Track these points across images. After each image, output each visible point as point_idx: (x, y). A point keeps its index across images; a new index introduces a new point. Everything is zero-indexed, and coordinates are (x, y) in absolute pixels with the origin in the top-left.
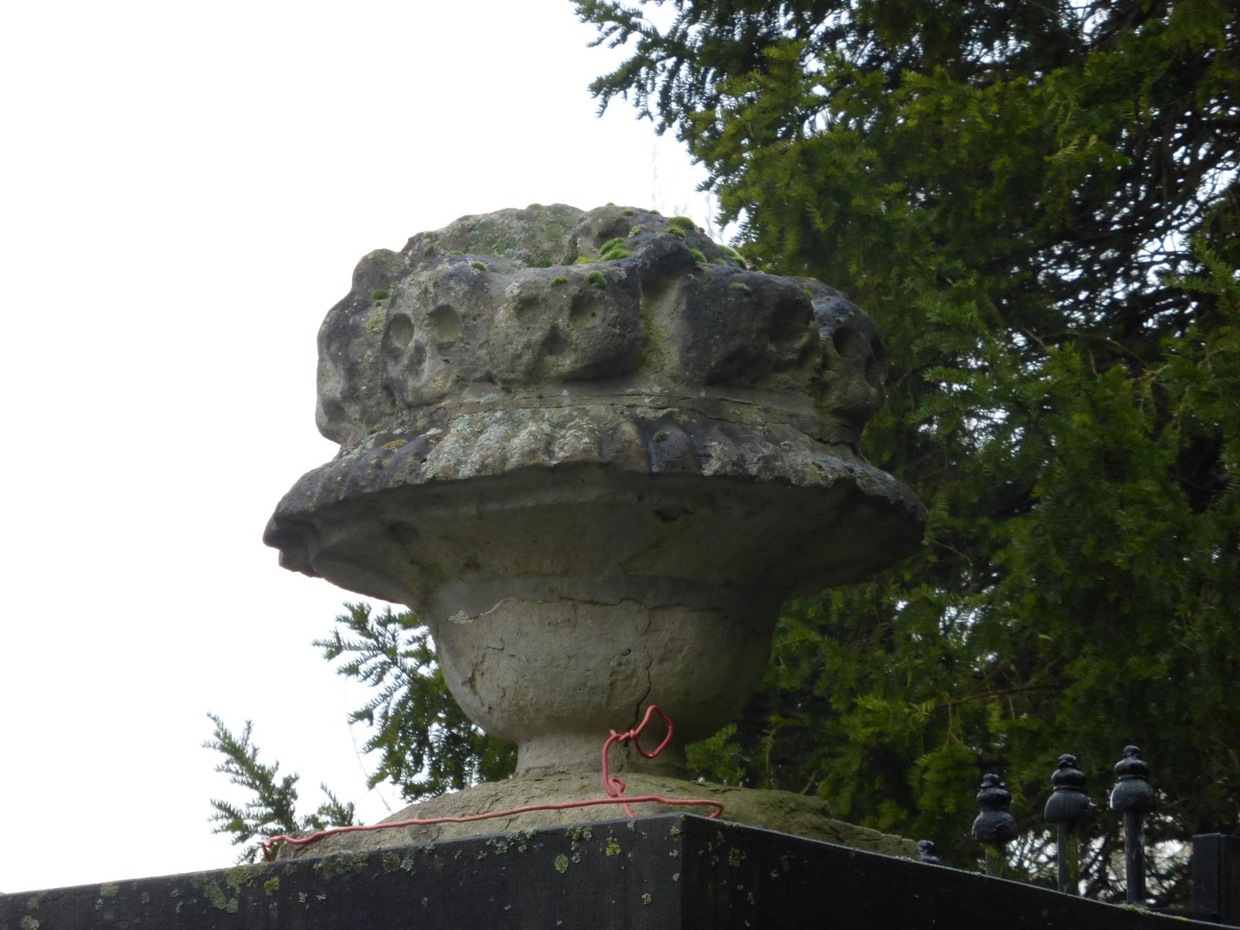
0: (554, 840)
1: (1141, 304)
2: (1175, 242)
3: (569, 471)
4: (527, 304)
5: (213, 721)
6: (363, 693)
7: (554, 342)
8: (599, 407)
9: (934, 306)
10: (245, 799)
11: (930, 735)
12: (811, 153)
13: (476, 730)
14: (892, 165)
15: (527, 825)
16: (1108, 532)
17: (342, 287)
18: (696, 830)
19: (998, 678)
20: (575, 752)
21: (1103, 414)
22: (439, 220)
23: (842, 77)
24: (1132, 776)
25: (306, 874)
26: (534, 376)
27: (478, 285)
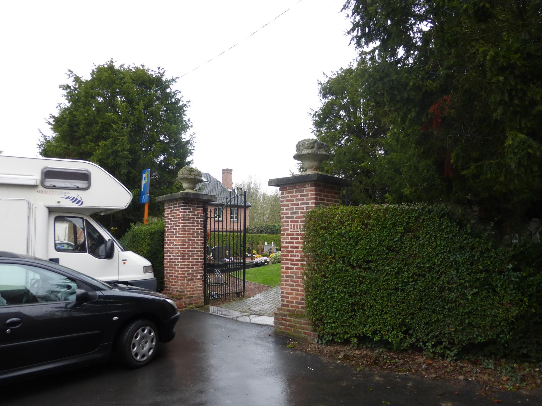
0: (310, 175)
1: (342, 145)
2: (343, 141)
3: (310, 154)
4: (307, 144)
5: (349, 42)
6: (298, 167)
7: (309, 146)
8: (312, 150)
9: (330, 145)
10: (291, 174)
11: (330, 169)
12: (323, 136)
13: (484, 5)
14: (327, 137)
15: (308, 174)
16: (340, 158)
17: (297, 143)
18: (318, 174)
19: (334, 166)
20: (311, 170)
21: (339, 151)
22: (302, 140)
23: (325, 132)
24: (122, 248)
25: (295, 177)
26: (308, 148)
27: (305, 143)
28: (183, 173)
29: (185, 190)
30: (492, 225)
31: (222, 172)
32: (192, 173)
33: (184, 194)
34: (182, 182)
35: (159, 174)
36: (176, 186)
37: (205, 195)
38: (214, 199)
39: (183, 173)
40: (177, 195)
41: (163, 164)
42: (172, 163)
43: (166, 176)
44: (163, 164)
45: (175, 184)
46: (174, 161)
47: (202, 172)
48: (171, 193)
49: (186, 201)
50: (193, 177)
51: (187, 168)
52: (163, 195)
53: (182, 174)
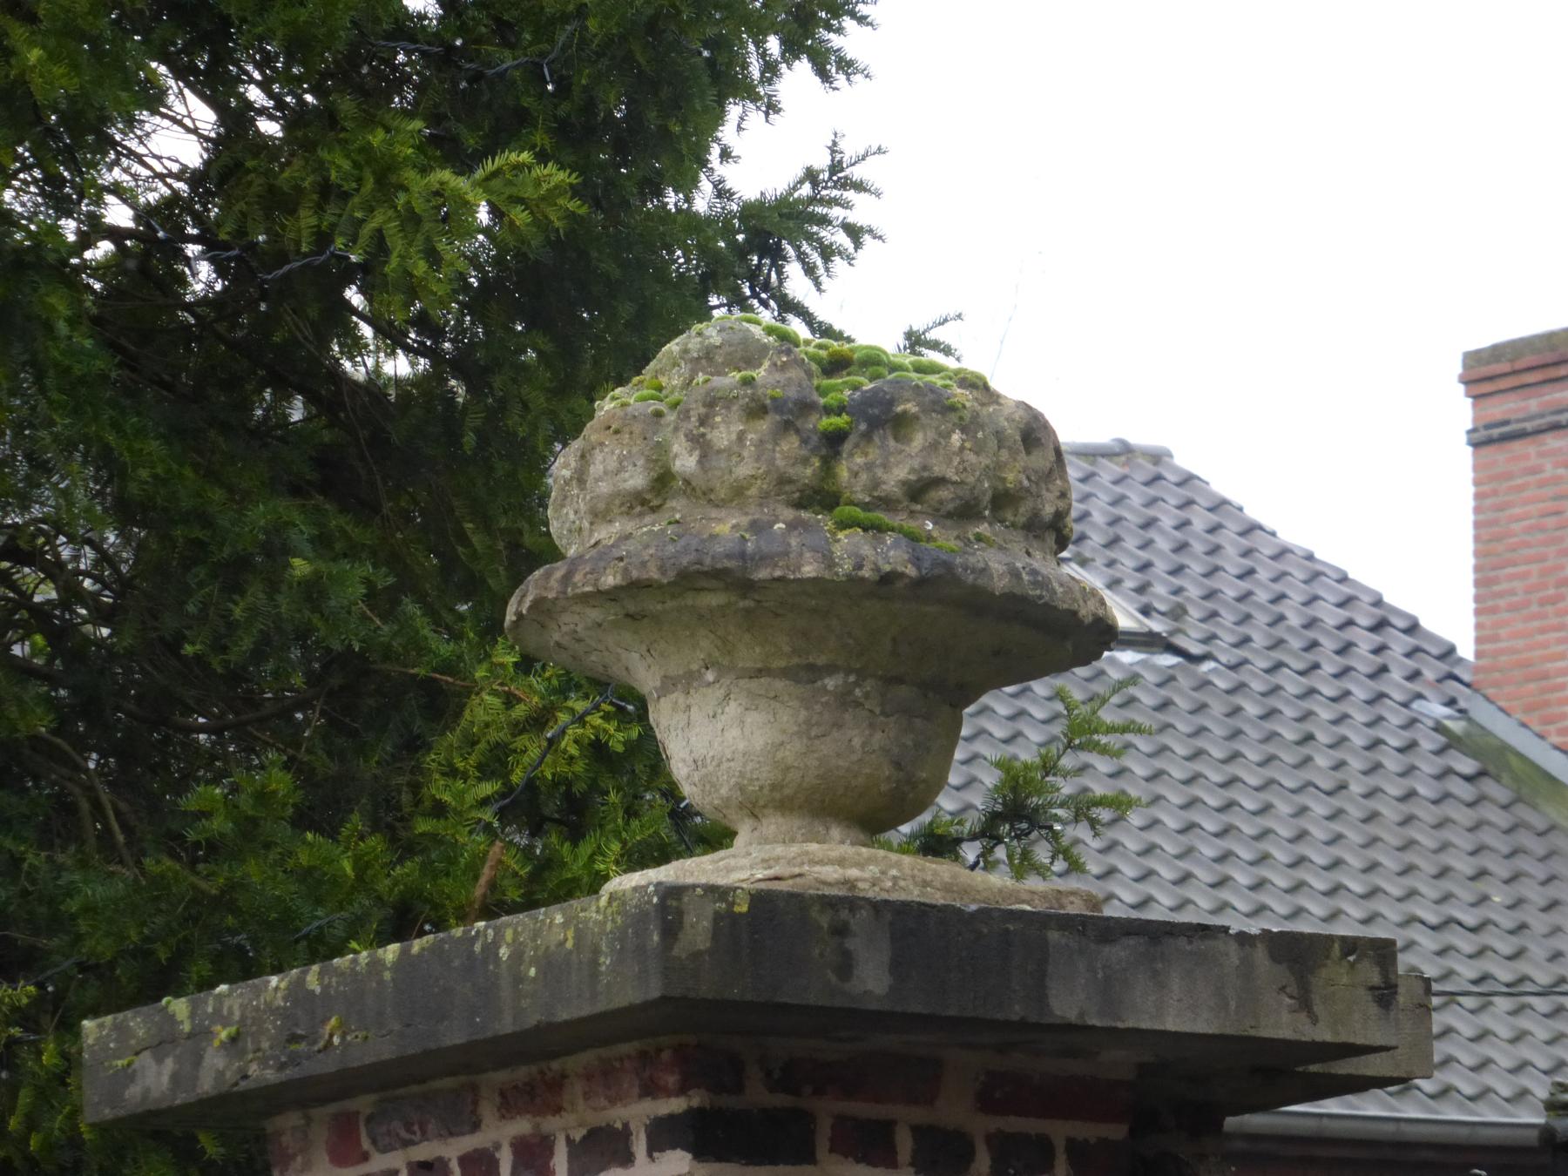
20: (773, 824)
28: (663, 481)
29: (716, 838)
30: (817, 464)
31: (1460, 412)
32: (850, 470)
33: (698, 930)
34: (646, 678)
35: (125, 513)
36: (496, 762)
37: (1157, 935)
38: (1364, 1027)
39: (663, 481)
40: (552, 965)
41: (203, 277)
42: (403, 256)
43: (277, 551)
44: (203, 277)
45: (484, 708)
46: (455, 218)
47: (1070, 431)
48: (401, 925)
49: (758, 1095)
50: (892, 555)
51: (748, 355)
52: (245, 969)
53: (641, 503)
